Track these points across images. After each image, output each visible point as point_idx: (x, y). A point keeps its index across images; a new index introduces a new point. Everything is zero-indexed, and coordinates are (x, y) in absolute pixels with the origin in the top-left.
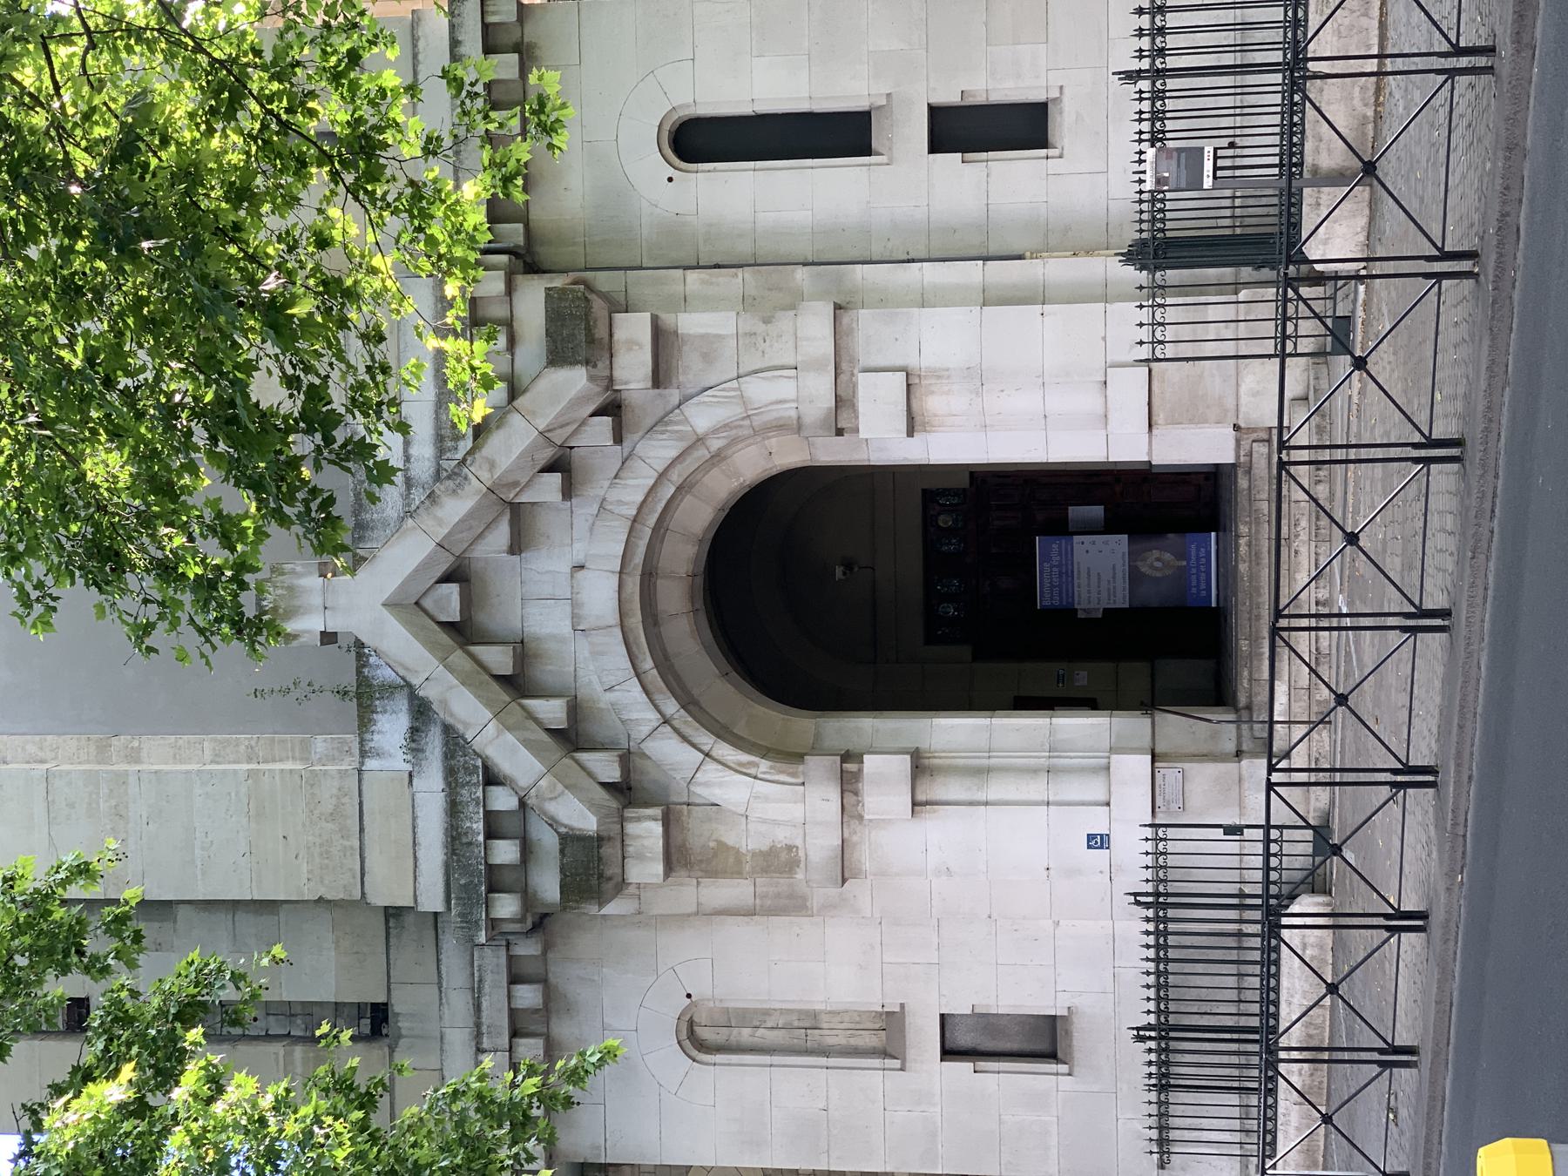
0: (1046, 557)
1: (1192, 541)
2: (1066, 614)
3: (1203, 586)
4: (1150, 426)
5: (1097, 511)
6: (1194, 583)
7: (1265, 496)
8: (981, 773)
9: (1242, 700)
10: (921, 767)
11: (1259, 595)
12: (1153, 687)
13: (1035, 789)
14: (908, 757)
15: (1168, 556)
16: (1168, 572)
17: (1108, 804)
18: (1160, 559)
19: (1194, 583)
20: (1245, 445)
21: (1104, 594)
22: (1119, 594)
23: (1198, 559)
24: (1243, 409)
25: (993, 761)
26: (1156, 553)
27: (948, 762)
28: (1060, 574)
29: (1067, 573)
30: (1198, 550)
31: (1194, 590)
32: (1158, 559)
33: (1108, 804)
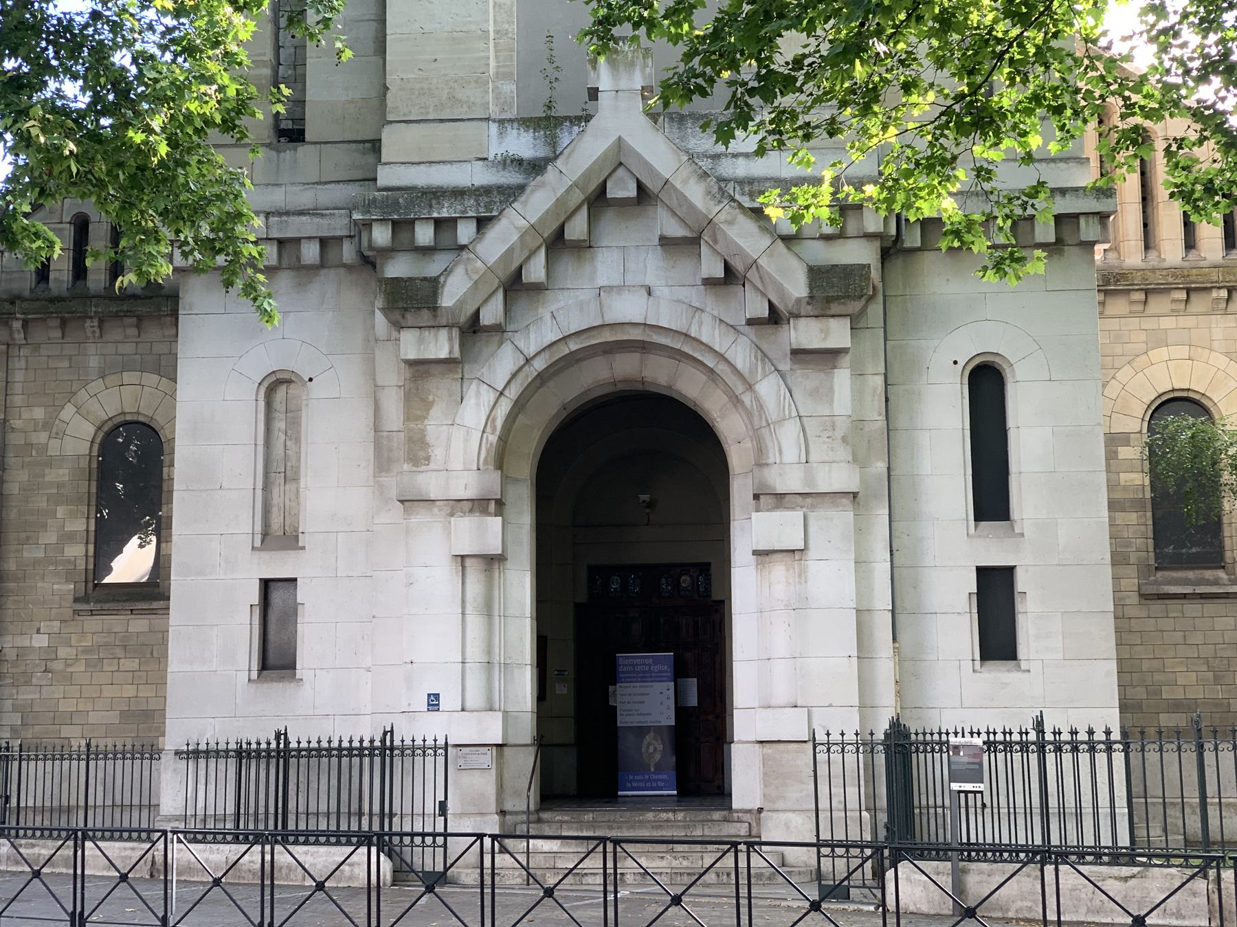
0: (656, 661)
1: (670, 775)
2: (611, 676)
3: (635, 784)
4: (762, 742)
5: (693, 701)
8: (488, 609)
9: (545, 815)
10: (492, 562)
13: (475, 652)
15: (658, 757)
17: (463, 710)
18: (656, 751)
19: (640, 777)
20: (747, 817)
22: (628, 719)
24: (775, 815)
25: (497, 618)
26: (660, 747)
32: (655, 749)
33: (463, 710)
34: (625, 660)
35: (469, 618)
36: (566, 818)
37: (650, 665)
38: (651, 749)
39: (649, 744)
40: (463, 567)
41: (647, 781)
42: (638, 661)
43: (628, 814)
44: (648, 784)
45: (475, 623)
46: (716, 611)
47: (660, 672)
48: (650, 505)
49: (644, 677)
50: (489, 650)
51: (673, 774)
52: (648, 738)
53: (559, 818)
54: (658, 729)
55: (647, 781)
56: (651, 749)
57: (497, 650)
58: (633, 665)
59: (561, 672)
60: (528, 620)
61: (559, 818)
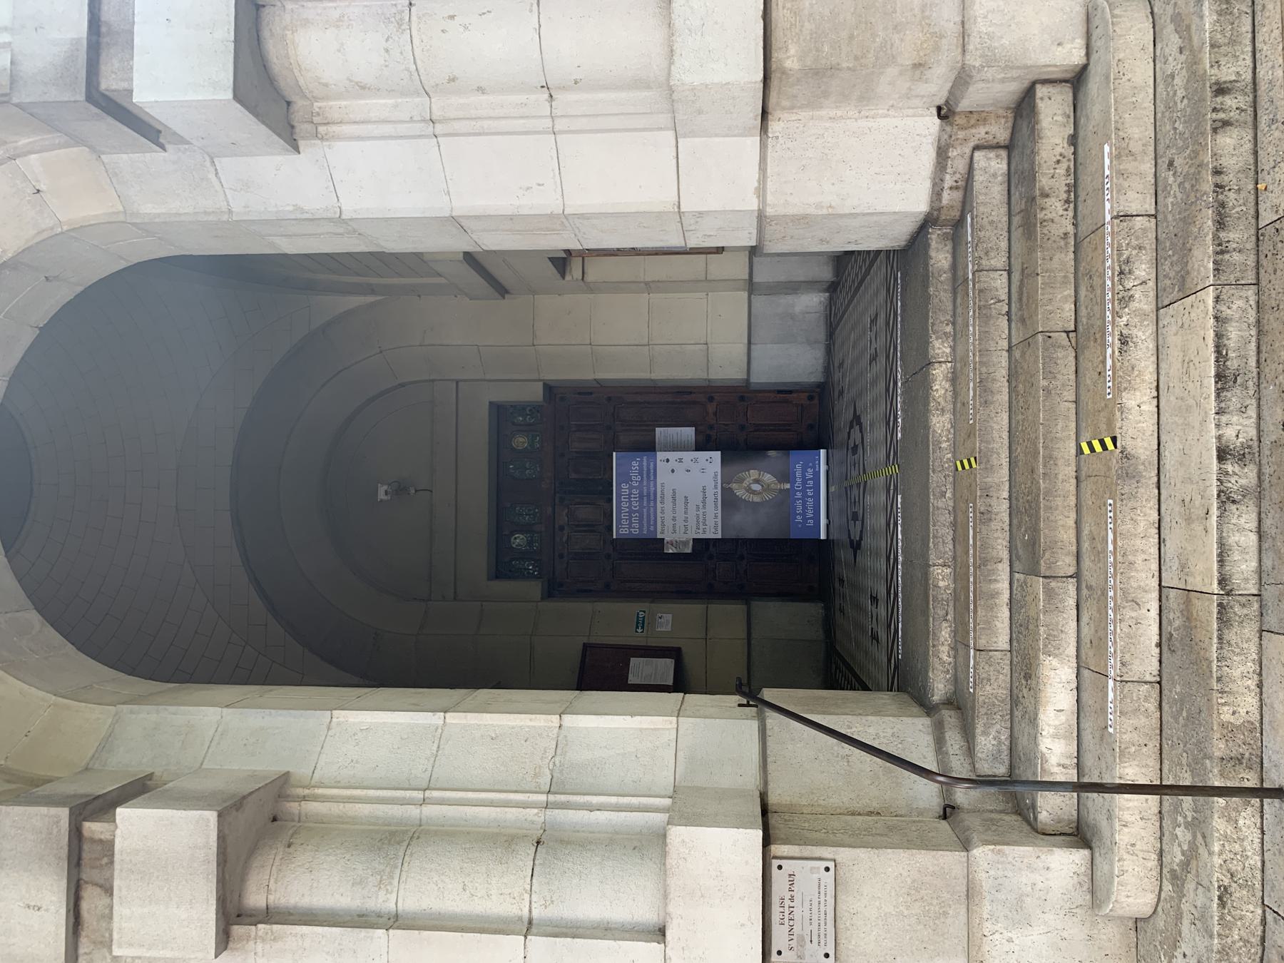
0: (625, 478)
1: (798, 462)
2: (650, 548)
3: (810, 514)
4: (765, 113)
5: (688, 433)
6: (799, 510)
7: (1000, 261)
8: (395, 841)
9: (939, 687)
10: (258, 824)
11: (989, 469)
12: (749, 634)
13: (499, 889)
14: (211, 816)
15: (768, 478)
16: (768, 497)
17: (660, 933)
18: (758, 481)
19: (799, 510)
20: (958, 163)
21: (692, 523)
22: (711, 522)
23: (804, 481)
24: (980, 27)
25: (429, 811)
26: (754, 474)
27: (336, 809)
28: (641, 497)
29: (649, 498)
30: (804, 471)
31: (799, 519)
32: (757, 481)
33: (660, 933)
34: (623, 527)
35: (1013, 325)
36: (945, 633)
37: (631, 488)
38: (756, 487)
40: (271, 916)
41: (805, 495)
42: (625, 505)
43: (935, 478)
45: (425, 886)
47: (641, 473)
50: (500, 841)
51: (794, 454)
53: (944, 652)
54: (726, 480)
55: (805, 495)
56: (756, 487)
57: (511, 814)
58: (631, 512)
59: (640, 623)
60: (453, 718)
61: (944, 652)
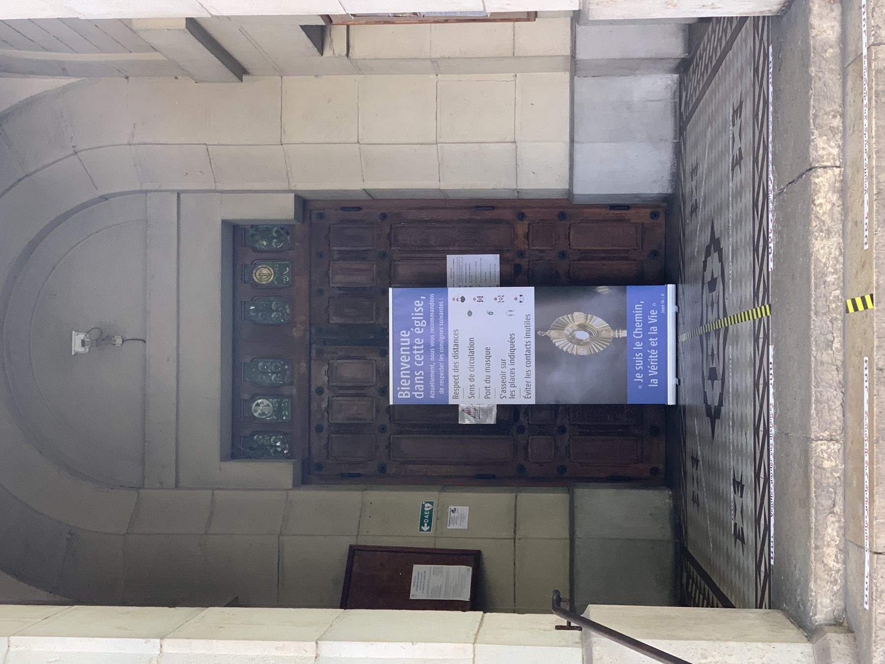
0: (406, 323)
1: (637, 298)
2: (439, 418)
3: (653, 371)
5: (491, 262)
15: (598, 323)
18: (585, 326)
26: (579, 317)
32: (583, 327)
34: (403, 389)
36: (832, 531)
37: (413, 336)
38: (583, 335)
39: (572, 339)
41: (645, 340)
42: (404, 360)
44: (653, 342)
46: (321, 216)
47: (426, 317)
48: (102, 339)
49: (438, 349)
51: (632, 291)
52: (560, 342)
54: (542, 326)
56: (583, 335)
58: (413, 369)
60: (172, 646)
